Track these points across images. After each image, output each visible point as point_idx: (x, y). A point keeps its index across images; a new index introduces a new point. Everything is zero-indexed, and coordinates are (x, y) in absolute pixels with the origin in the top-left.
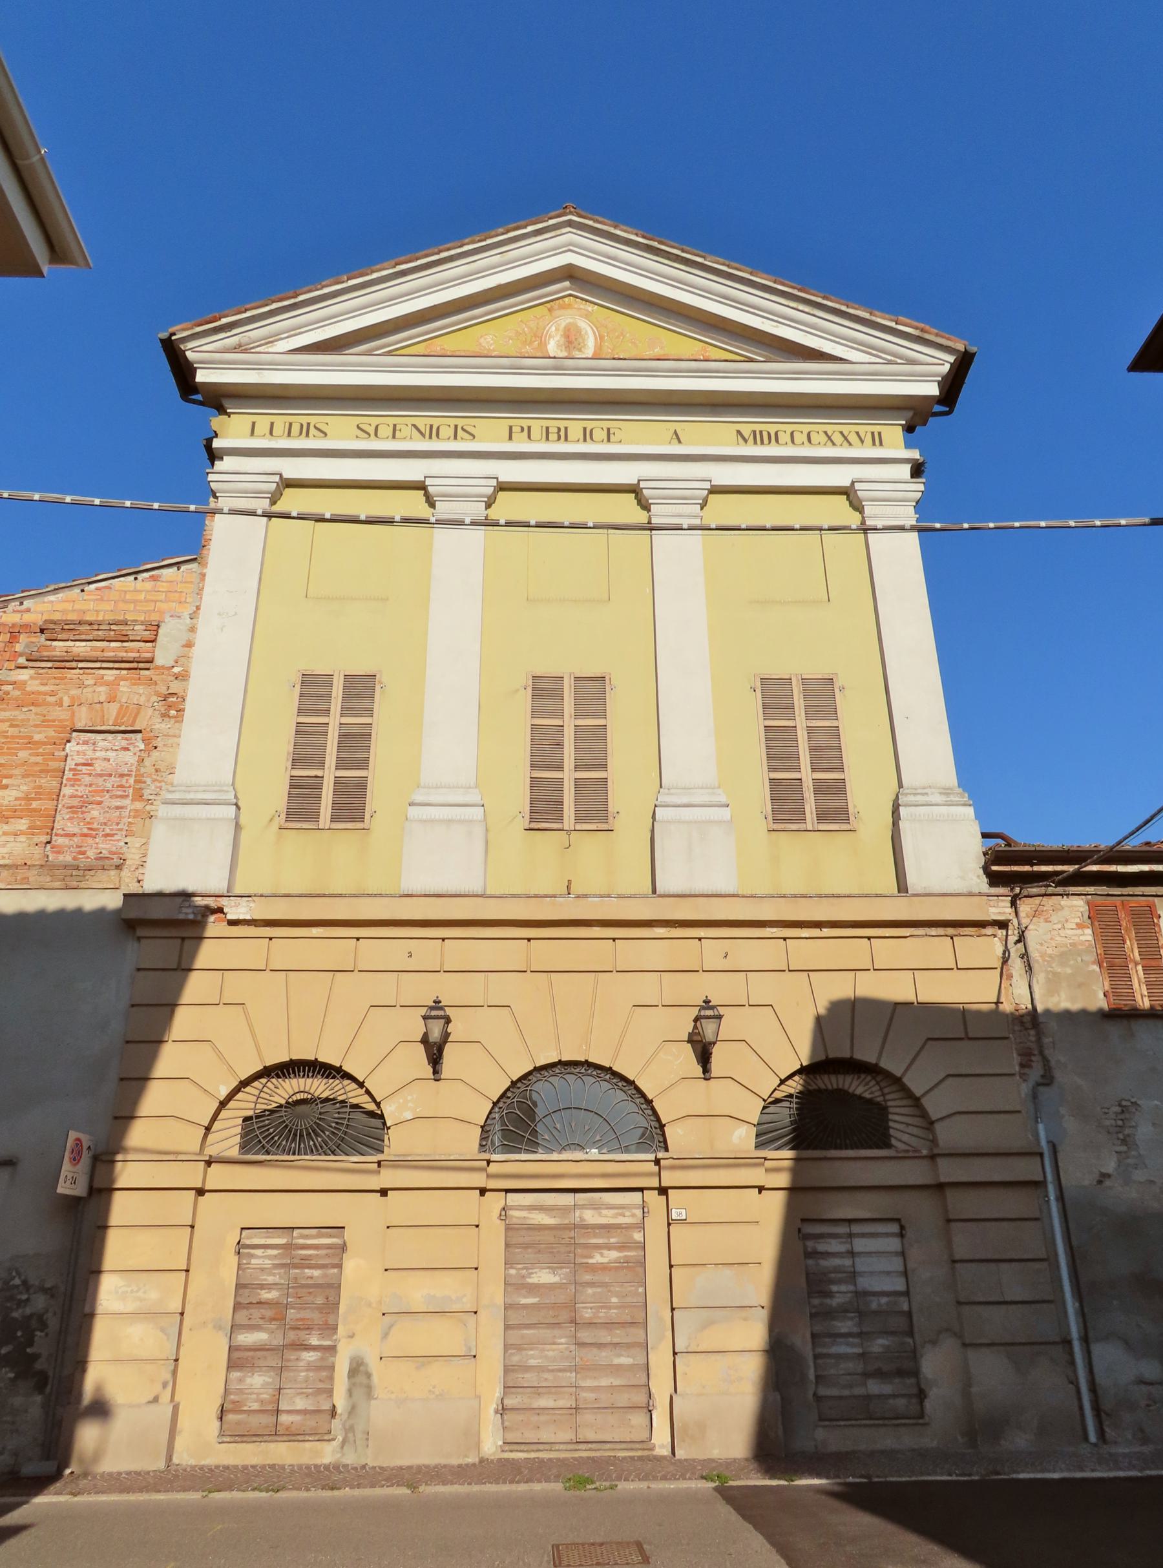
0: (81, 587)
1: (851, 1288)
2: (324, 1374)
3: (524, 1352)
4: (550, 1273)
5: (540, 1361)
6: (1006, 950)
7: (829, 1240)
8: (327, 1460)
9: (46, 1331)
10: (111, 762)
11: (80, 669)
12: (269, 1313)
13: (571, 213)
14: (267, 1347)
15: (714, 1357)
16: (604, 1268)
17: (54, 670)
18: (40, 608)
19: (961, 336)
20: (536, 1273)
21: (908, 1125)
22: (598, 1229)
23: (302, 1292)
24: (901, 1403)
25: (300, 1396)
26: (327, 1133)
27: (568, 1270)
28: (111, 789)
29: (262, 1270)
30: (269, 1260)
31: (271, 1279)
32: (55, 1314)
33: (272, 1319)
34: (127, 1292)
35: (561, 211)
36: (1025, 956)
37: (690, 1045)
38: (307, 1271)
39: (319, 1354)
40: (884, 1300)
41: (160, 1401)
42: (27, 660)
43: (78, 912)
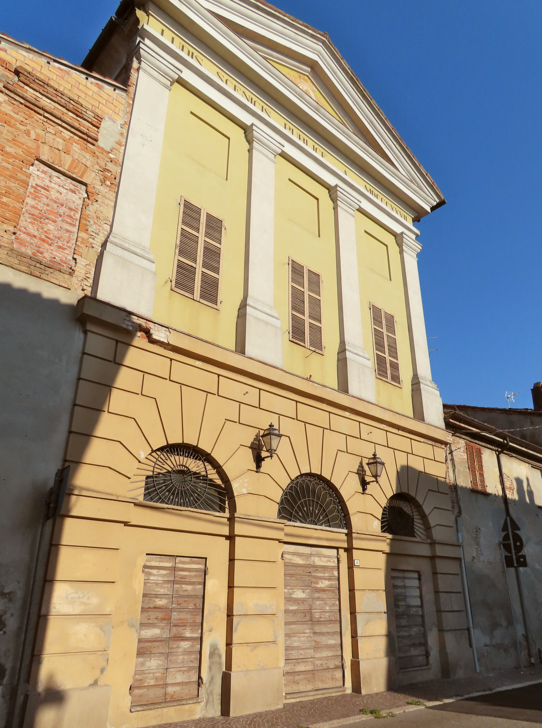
0: (49, 60)
1: (405, 603)
2: (194, 656)
3: (292, 638)
4: (302, 592)
5: (298, 643)
6: (446, 456)
7: (398, 580)
8: (197, 716)
9: (4, 630)
10: (62, 196)
11: (45, 117)
12: (160, 615)
13: (326, 38)
14: (159, 639)
15: (371, 638)
16: (323, 590)
17: (23, 106)
18: (14, 54)
19: (444, 196)
20: (296, 591)
21: (420, 528)
22: (321, 568)
23: (181, 600)
24: (421, 658)
25: (180, 673)
26: (167, 493)
27: (309, 591)
28: (62, 214)
29: (157, 584)
30: (161, 577)
31: (162, 591)
32: (12, 615)
33: (163, 619)
34: (75, 598)
35: (323, 33)
36: (452, 460)
37: (357, 475)
38: (184, 586)
39: (190, 643)
40: (414, 609)
41: (99, 684)
42: (4, 87)
43: (37, 296)
